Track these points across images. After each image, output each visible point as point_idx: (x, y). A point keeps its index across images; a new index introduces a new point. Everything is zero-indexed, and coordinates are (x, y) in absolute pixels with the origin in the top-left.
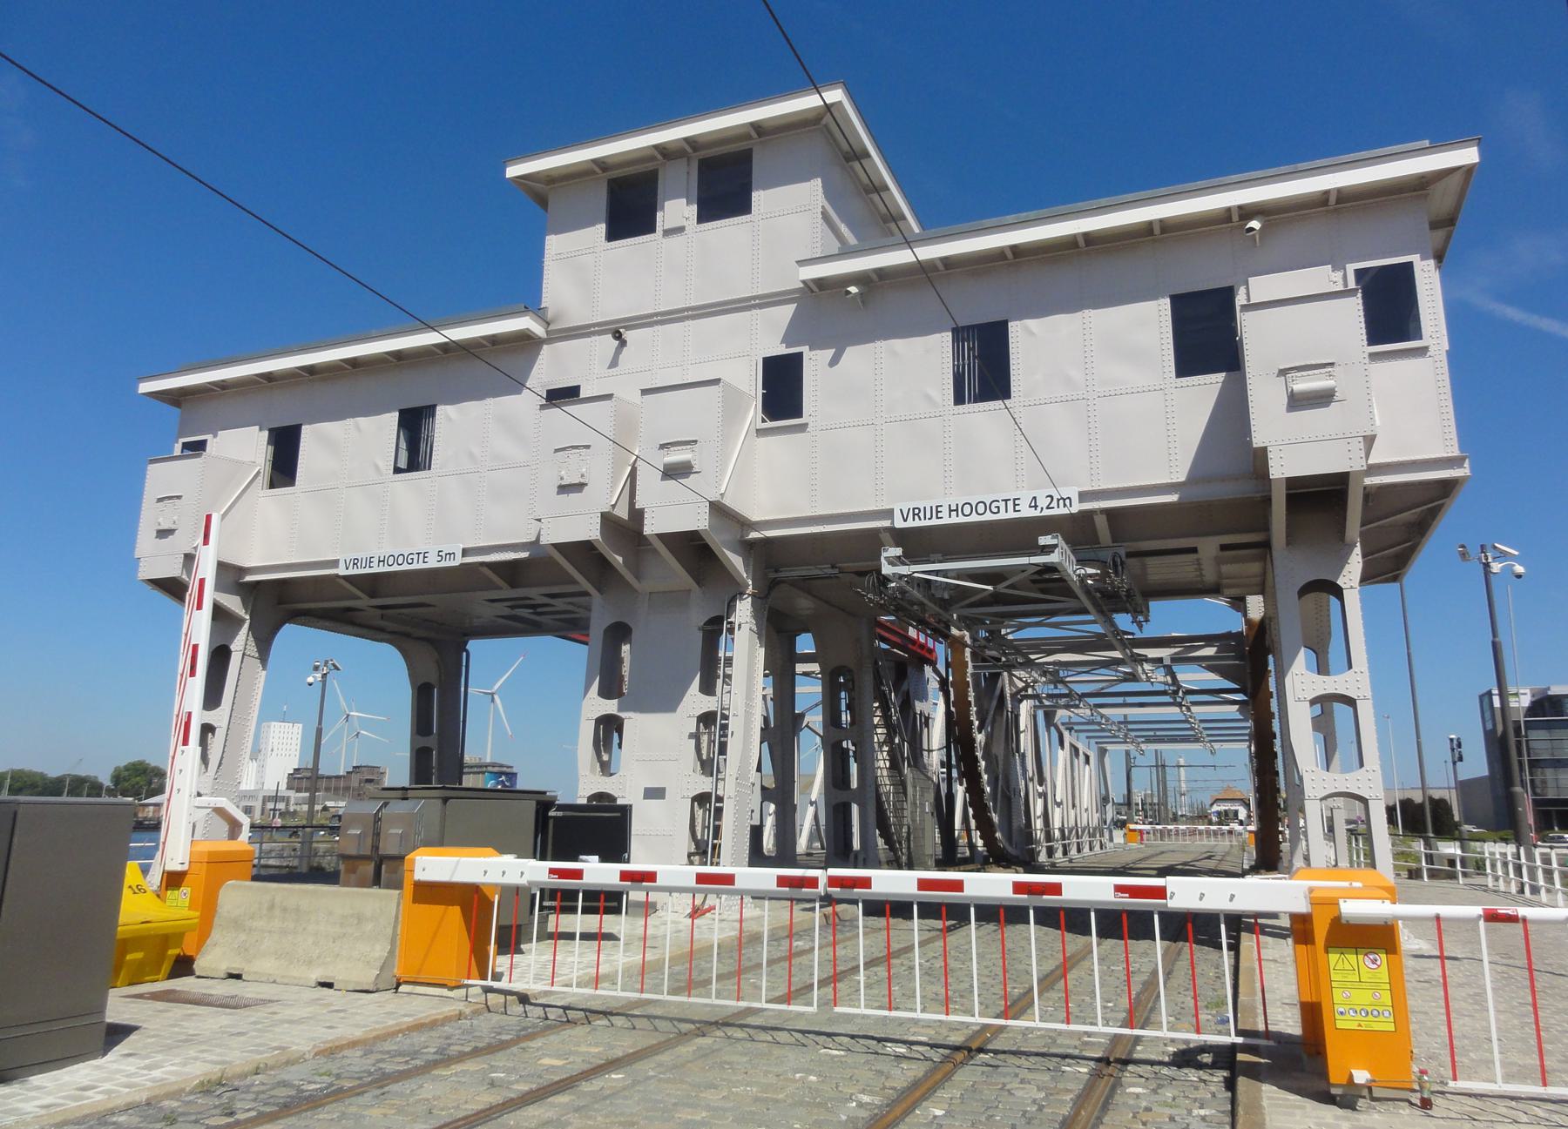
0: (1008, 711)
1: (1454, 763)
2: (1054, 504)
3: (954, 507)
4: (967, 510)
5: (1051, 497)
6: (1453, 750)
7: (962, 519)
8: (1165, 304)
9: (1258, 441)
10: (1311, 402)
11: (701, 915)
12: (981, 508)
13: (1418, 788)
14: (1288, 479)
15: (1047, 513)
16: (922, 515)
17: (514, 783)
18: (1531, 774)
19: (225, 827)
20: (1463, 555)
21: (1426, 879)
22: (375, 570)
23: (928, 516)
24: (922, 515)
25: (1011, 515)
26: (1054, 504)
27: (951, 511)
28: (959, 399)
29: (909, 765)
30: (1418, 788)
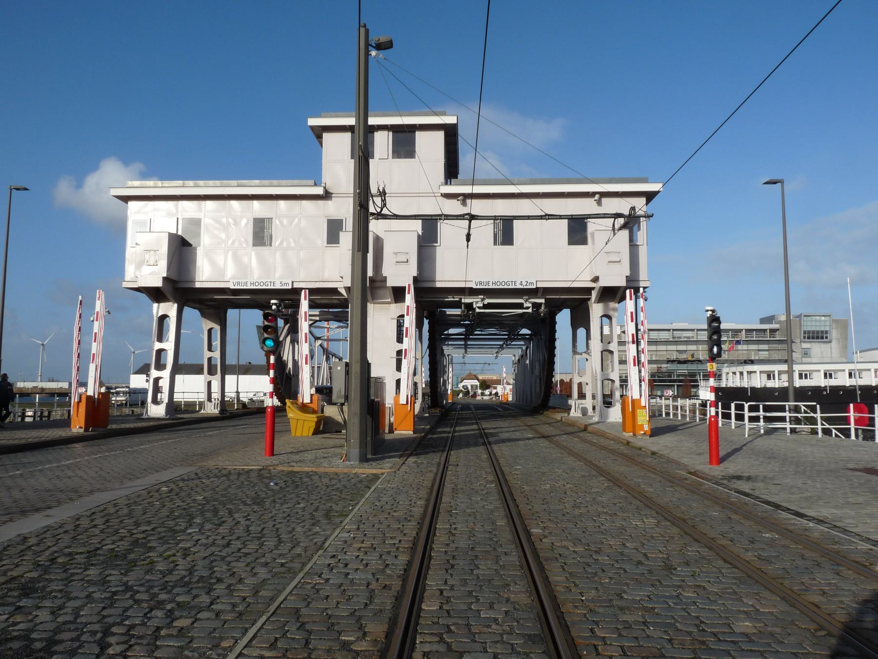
0: (638, 362)
2: (528, 284)
4: (498, 284)
7: (497, 287)
10: (459, 218)
12: (262, 284)
15: (525, 287)
22: (491, 287)
25: (513, 287)
26: (528, 284)
28: (495, 244)
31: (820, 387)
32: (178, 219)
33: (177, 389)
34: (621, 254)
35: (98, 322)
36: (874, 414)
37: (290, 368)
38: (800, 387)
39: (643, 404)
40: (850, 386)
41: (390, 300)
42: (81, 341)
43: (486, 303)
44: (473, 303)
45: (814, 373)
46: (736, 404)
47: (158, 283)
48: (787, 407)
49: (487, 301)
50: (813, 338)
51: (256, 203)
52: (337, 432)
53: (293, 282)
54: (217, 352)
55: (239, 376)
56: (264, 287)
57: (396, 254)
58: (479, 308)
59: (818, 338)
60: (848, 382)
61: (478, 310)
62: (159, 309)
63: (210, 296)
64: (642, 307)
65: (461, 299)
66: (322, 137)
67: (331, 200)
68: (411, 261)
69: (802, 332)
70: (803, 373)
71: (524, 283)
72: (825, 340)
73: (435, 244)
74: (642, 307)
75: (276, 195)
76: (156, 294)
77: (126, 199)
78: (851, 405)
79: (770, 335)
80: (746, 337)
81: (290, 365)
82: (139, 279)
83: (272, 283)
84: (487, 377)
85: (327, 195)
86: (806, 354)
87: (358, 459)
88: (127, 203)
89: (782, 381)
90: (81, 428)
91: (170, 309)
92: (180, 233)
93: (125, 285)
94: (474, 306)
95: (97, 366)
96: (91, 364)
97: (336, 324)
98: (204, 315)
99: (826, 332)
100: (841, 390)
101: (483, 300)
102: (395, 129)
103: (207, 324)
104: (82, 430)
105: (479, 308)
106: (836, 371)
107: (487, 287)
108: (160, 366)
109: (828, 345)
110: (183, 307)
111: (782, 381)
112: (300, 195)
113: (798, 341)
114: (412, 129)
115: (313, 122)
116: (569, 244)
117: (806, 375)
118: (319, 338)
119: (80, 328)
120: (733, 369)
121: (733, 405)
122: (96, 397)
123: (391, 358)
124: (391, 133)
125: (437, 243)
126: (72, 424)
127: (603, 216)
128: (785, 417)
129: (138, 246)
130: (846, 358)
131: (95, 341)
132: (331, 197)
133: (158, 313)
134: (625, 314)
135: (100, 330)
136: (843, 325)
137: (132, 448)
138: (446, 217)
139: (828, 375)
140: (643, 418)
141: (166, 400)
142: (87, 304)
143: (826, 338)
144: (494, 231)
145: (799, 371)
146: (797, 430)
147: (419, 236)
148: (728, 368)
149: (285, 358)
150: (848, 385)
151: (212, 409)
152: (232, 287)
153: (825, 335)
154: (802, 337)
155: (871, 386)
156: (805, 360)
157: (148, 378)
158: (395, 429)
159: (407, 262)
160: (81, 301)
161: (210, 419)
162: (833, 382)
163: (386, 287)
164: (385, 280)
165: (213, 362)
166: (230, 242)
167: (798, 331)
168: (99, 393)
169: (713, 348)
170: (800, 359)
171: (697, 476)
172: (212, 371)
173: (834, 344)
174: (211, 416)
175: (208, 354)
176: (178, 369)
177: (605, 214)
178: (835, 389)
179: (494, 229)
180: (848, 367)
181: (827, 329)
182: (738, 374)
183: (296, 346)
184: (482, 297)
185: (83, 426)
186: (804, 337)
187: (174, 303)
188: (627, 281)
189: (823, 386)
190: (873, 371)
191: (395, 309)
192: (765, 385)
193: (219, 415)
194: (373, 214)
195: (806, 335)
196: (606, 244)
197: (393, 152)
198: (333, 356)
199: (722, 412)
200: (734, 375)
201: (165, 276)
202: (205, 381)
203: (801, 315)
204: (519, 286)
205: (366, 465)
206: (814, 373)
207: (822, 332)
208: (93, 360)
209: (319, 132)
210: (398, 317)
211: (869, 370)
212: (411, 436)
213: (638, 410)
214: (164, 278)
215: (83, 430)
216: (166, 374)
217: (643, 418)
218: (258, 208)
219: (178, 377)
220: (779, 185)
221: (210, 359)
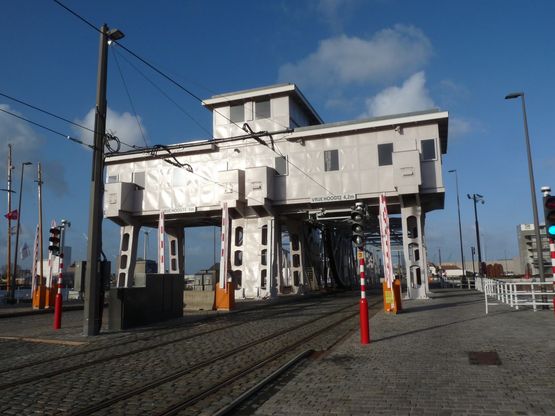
1: (473, 254)
2: (350, 197)
5: (349, 196)
6: (472, 250)
7: (327, 201)
9: (246, 198)
11: (73, 345)
15: (348, 199)
18: (537, 296)
20: (469, 197)
21: (461, 288)
26: (350, 197)
27: (324, 199)
28: (326, 170)
29: (318, 244)
34: (413, 169)
43: (325, 213)
49: (326, 211)
51: (328, 140)
53: (356, 195)
57: (253, 183)
58: (319, 217)
61: (318, 219)
65: (308, 212)
71: (347, 197)
73: (434, 160)
84: (445, 264)
90: (37, 306)
91: (130, 230)
92: (134, 182)
101: (323, 211)
102: (256, 99)
104: (38, 308)
105: (319, 217)
107: (321, 202)
110: (425, 214)
112: (357, 130)
114: (266, 98)
124: (254, 103)
125: (435, 158)
128: (531, 296)
133: (124, 233)
146: (549, 307)
147: (420, 154)
152: (312, 202)
158: (218, 307)
159: (413, 174)
184: (322, 209)
185: (38, 305)
191: (261, 222)
201: (120, 209)
204: (343, 199)
209: (212, 107)
210: (263, 227)
212: (209, 313)
214: (265, 199)
215: (38, 307)
218: (383, 138)
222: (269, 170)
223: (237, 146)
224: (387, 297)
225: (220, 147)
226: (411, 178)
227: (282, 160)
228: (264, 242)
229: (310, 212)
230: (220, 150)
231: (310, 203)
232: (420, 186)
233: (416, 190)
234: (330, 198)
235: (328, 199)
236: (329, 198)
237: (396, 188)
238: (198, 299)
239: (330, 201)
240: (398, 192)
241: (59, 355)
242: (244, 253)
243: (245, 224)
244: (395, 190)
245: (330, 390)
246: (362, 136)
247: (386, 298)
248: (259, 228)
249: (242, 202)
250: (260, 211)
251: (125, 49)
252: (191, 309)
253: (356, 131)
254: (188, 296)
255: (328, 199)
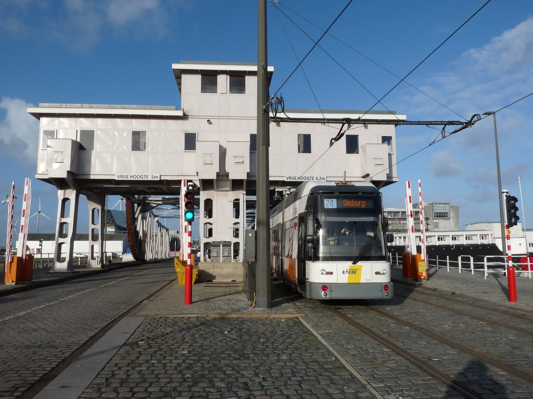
2: (321, 179)
3: (131, 176)
8: (256, 133)
10: (330, 121)
13: (248, 118)
14: (232, 179)
16: (123, 177)
17: (310, 259)
19: (67, 202)
23: (125, 177)
24: (123, 177)
26: (321, 179)
27: (298, 178)
28: (299, 152)
30: (248, 118)
31: (450, 245)
32: (77, 130)
33: (75, 251)
35: (26, 202)
36: (470, 262)
37: (140, 236)
38: (439, 245)
39: (423, 258)
40: (467, 245)
41: (229, 189)
42: (14, 216)
44: (283, 191)
45: (446, 237)
46: (462, 257)
47: (64, 175)
48: (505, 258)
50: (440, 217)
51: (134, 121)
52: (208, 281)
53: (160, 176)
54: (98, 225)
55: (106, 241)
56: (140, 179)
57: (235, 157)
59: (442, 217)
60: (438, 243)
62: (61, 194)
63: (100, 185)
64: (420, 193)
65: (275, 188)
66: (180, 78)
67: (188, 120)
68: (245, 162)
69: (434, 213)
70: (440, 237)
72: (446, 218)
74: (420, 193)
75: (149, 115)
76: (60, 183)
77: (38, 116)
78: (448, 257)
79: (415, 215)
80: (402, 216)
81: (141, 234)
82: (50, 172)
83: (146, 176)
85: (185, 117)
86: (436, 226)
87: (266, 306)
88: (39, 119)
89: (428, 242)
90: (13, 281)
91: (71, 194)
92: (78, 140)
93: (37, 176)
94: (284, 193)
95: (25, 234)
96: (20, 234)
97: (172, 207)
98: (89, 198)
99: (447, 213)
100: (461, 247)
102: (231, 74)
103: (93, 205)
104: (14, 284)
106: (458, 236)
108: (62, 235)
109: (448, 221)
110: (79, 195)
111: (428, 242)
113: (431, 218)
115: (175, 66)
116: (347, 153)
117: (442, 238)
118: (157, 216)
119: (13, 206)
120: (400, 235)
121: (460, 258)
122: (24, 258)
123: (230, 228)
124: (228, 77)
126: (6, 278)
127: (441, 123)
129: (49, 149)
130: (458, 228)
131: (23, 216)
132: (188, 118)
134: (406, 197)
135: (27, 207)
136: (456, 209)
137: (63, 298)
138: (328, 121)
139: (454, 238)
140: (422, 268)
141: (67, 259)
142: (18, 189)
143: (447, 216)
144: (298, 144)
145: (438, 236)
148: (396, 235)
149: (138, 229)
150: (465, 244)
151: (95, 265)
152: (117, 179)
153: (446, 215)
154: (434, 216)
155: (478, 244)
156: (435, 229)
157: (41, 243)
159: (243, 162)
160: (14, 186)
161: (95, 273)
162: (457, 242)
163: (228, 180)
164: (227, 175)
165: (95, 233)
166: (115, 147)
167: (432, 212)
168: (26, 255)
169: (511, 219)
170: (433, 229)
171: (513, 309)
172: (95, 238)
173: (451, 220)
174: (93, 271)
175: (92, 226)
176: (76, 237)
177: (441, 122)
178: (458, 247)
179: (298, 142)
180: (465, 233)
181: (448, 211)
182: (402, 238)
183: (145, 221)
184: (289, 187)
186: (435, 216)
187: (73, 190)
188: (387, 177)
189: (451, 245)
190: (479, 235)
191: (233, 195)
192: (396, 244)
193: (101, 269)
194: (272, 118)
195: (436, 215)
196: (430, 145)
197: (230, 90)
198: (163, 228)
199: (449, 262)
200: (400, 239)
201: (69, 170)
202: (90, 245)
203: (433, 203)
205: (275, 309)
206: (446, 237)
207: (445, 213)
208: (22, 230)
209: (179, 74)
210: (234, 200)
211: (477, 235)
213: (419, 263)
214: (68, 172)
215: (15, 283)
216: (68, 240)
217: (422, 268)
219: (76, 242)
220: (492, 116)
221: (93, 230)
222: (74, 143)
223: (210, 117)
224: (420, 267)
225: (189, 116)
226: (240, 166)
227: (88, 135)
228: (237, 216)
229: (277, 190)
230: (189, 119)
231: (284, 181)
232: (248, 173)
233: (244, 177)
234: (137, 177)
235: (135, 177)
236: (302, 178)
237: (197, 173)
238: (228, 270)
239: (137, 179)
240: (199, 177)
241: (435, 326)
242: (69, 224)
243: (216, 196)
244: (196, 175)
245: (119, 365)
246: (118, 121)
247: (419, 268)
248: (230, 202)
249: (222, 175)
250: (237, 184)
251: (478, 11)
252: (222, 281)
253: (130, 115)
254: (215, 268)
255: (135, 177)
